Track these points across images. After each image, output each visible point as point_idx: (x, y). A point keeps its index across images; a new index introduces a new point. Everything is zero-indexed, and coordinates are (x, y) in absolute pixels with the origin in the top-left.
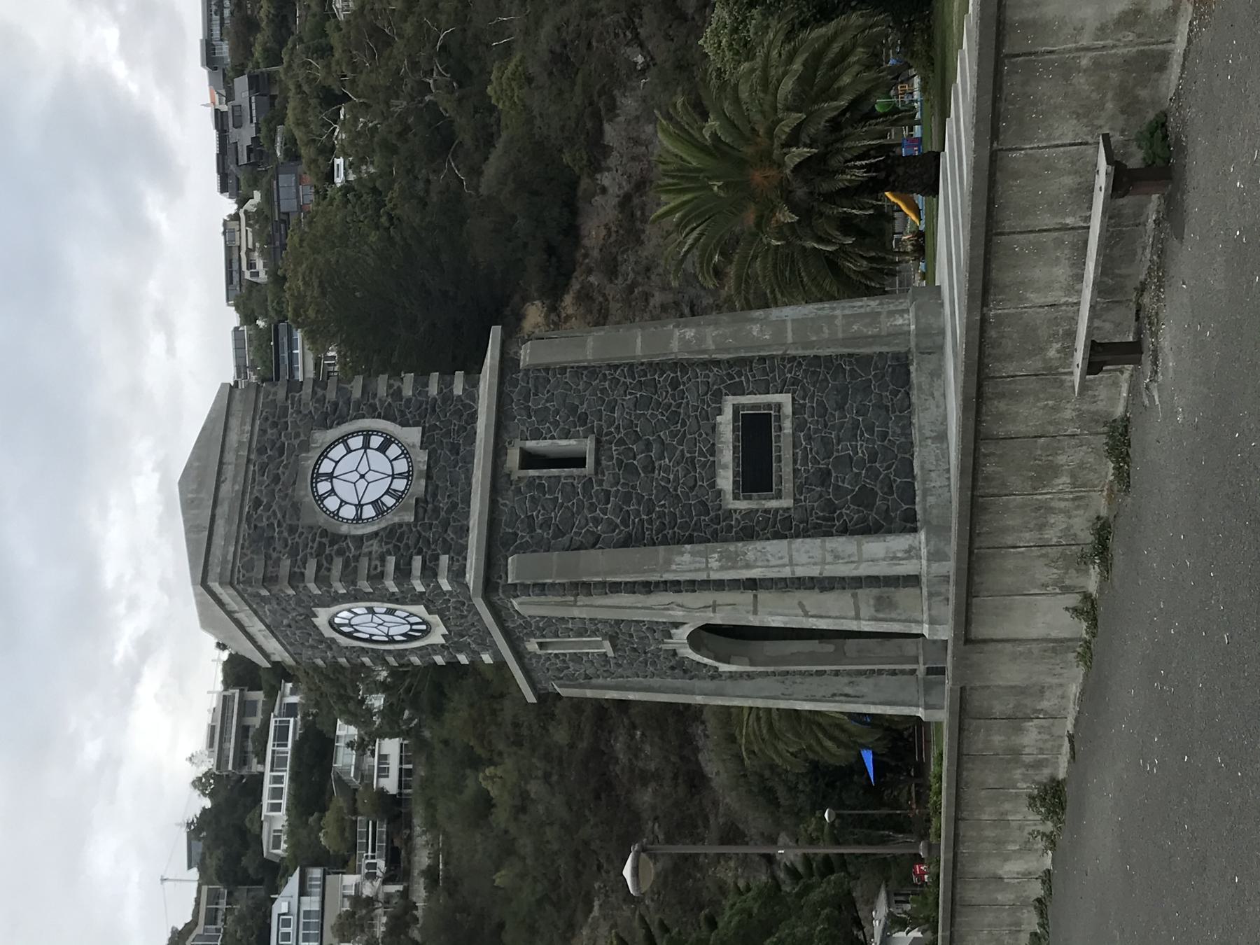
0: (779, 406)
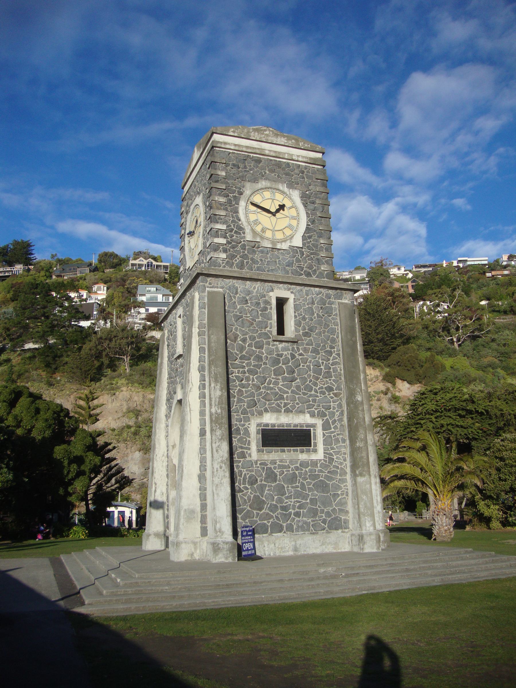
0: (315, 451)
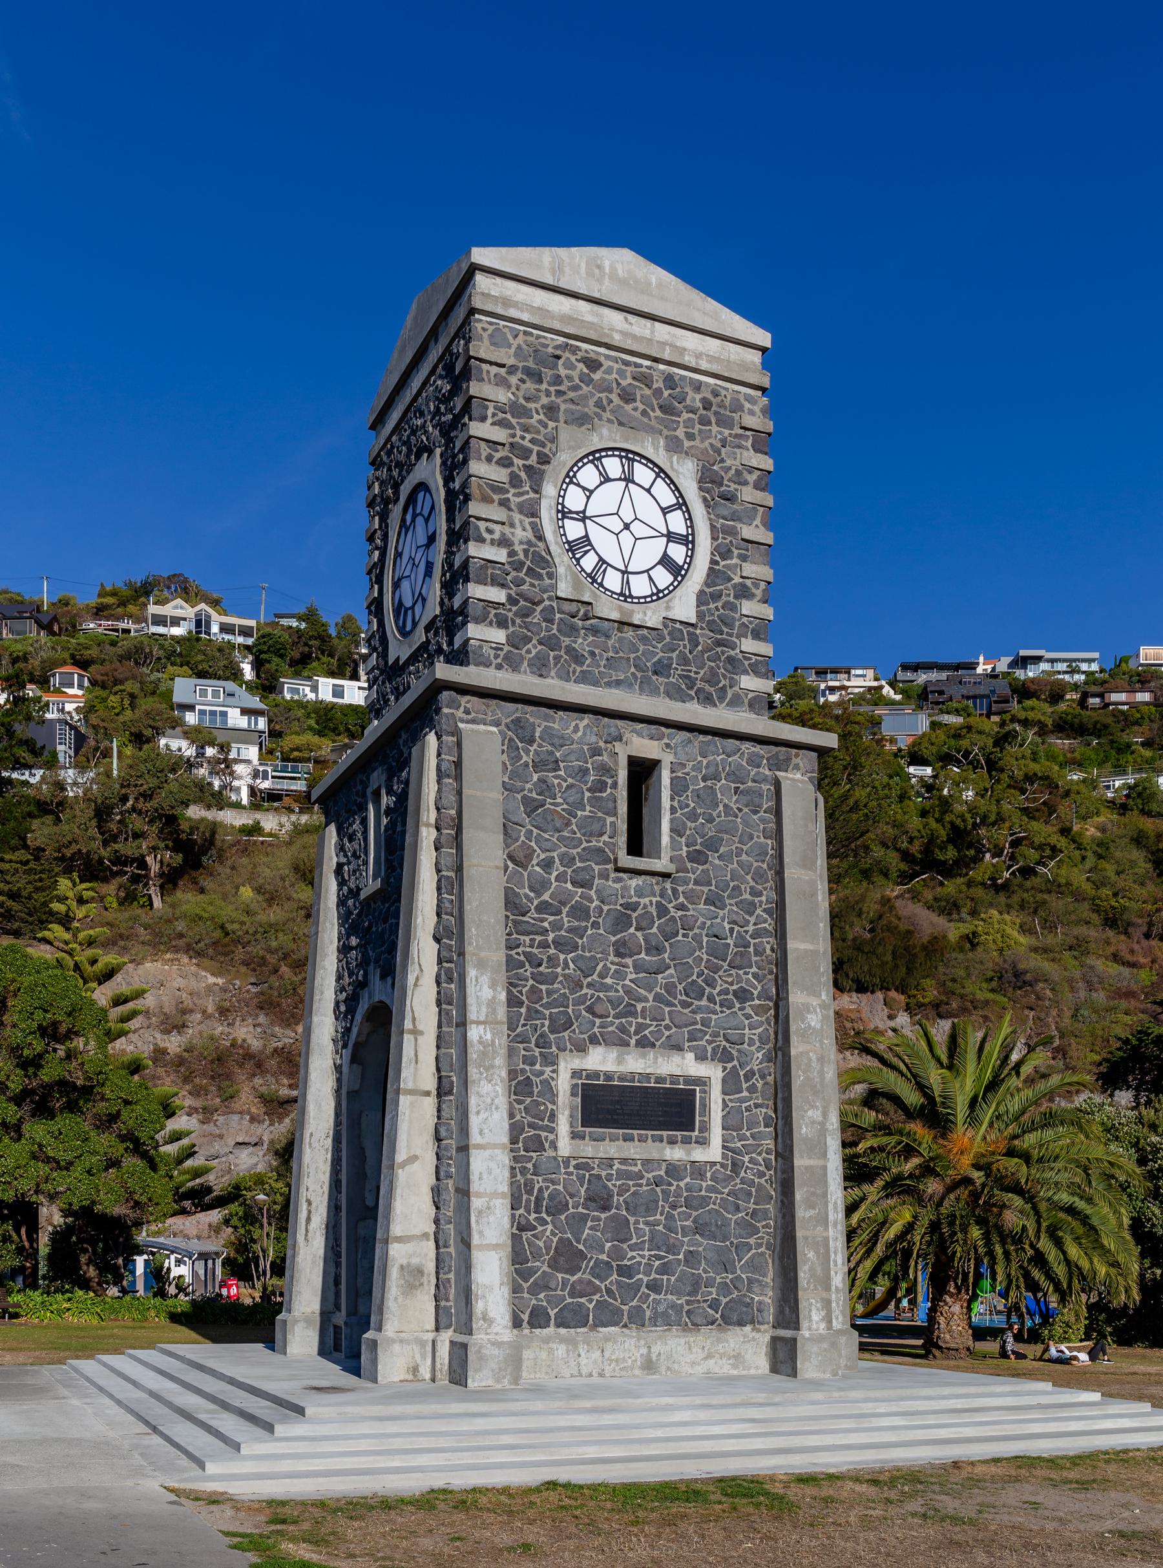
0: (703, 1142)
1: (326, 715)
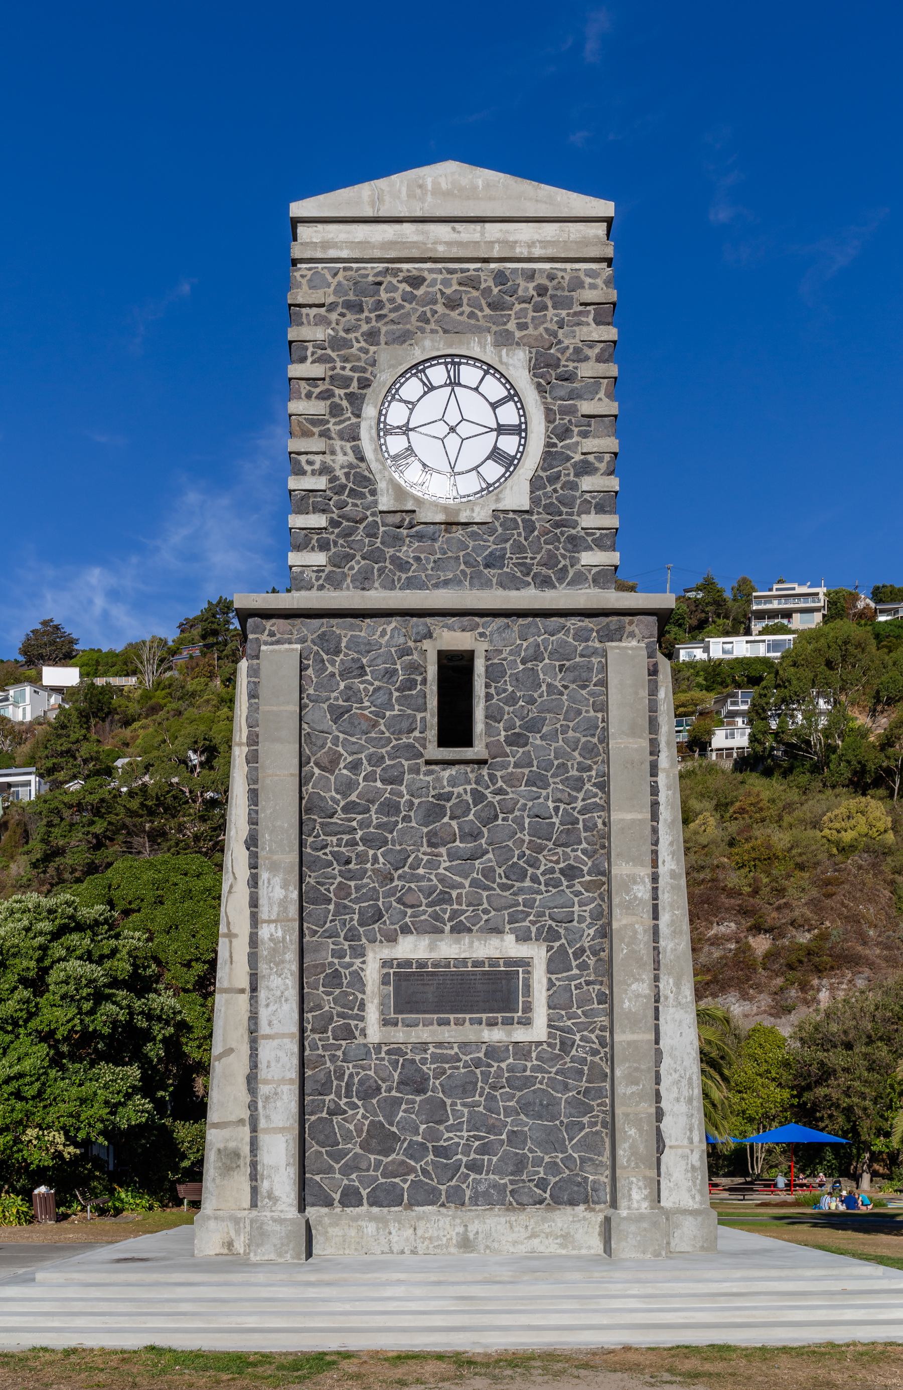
0: (526, 1022)
1: (714, 670)
